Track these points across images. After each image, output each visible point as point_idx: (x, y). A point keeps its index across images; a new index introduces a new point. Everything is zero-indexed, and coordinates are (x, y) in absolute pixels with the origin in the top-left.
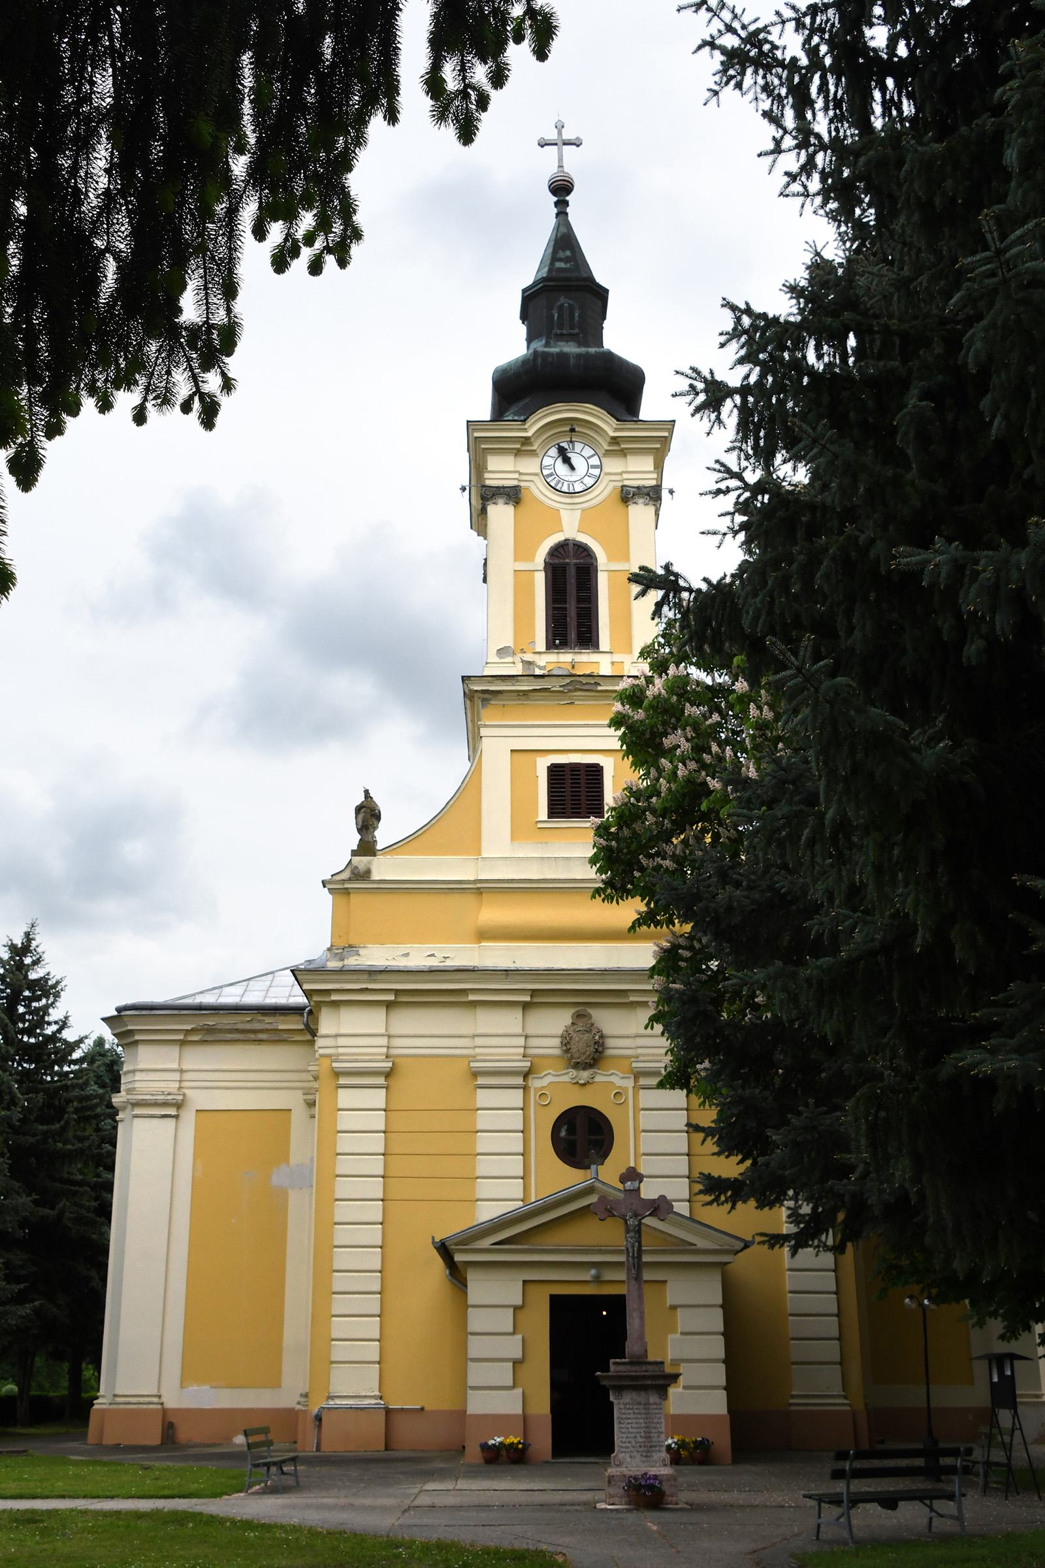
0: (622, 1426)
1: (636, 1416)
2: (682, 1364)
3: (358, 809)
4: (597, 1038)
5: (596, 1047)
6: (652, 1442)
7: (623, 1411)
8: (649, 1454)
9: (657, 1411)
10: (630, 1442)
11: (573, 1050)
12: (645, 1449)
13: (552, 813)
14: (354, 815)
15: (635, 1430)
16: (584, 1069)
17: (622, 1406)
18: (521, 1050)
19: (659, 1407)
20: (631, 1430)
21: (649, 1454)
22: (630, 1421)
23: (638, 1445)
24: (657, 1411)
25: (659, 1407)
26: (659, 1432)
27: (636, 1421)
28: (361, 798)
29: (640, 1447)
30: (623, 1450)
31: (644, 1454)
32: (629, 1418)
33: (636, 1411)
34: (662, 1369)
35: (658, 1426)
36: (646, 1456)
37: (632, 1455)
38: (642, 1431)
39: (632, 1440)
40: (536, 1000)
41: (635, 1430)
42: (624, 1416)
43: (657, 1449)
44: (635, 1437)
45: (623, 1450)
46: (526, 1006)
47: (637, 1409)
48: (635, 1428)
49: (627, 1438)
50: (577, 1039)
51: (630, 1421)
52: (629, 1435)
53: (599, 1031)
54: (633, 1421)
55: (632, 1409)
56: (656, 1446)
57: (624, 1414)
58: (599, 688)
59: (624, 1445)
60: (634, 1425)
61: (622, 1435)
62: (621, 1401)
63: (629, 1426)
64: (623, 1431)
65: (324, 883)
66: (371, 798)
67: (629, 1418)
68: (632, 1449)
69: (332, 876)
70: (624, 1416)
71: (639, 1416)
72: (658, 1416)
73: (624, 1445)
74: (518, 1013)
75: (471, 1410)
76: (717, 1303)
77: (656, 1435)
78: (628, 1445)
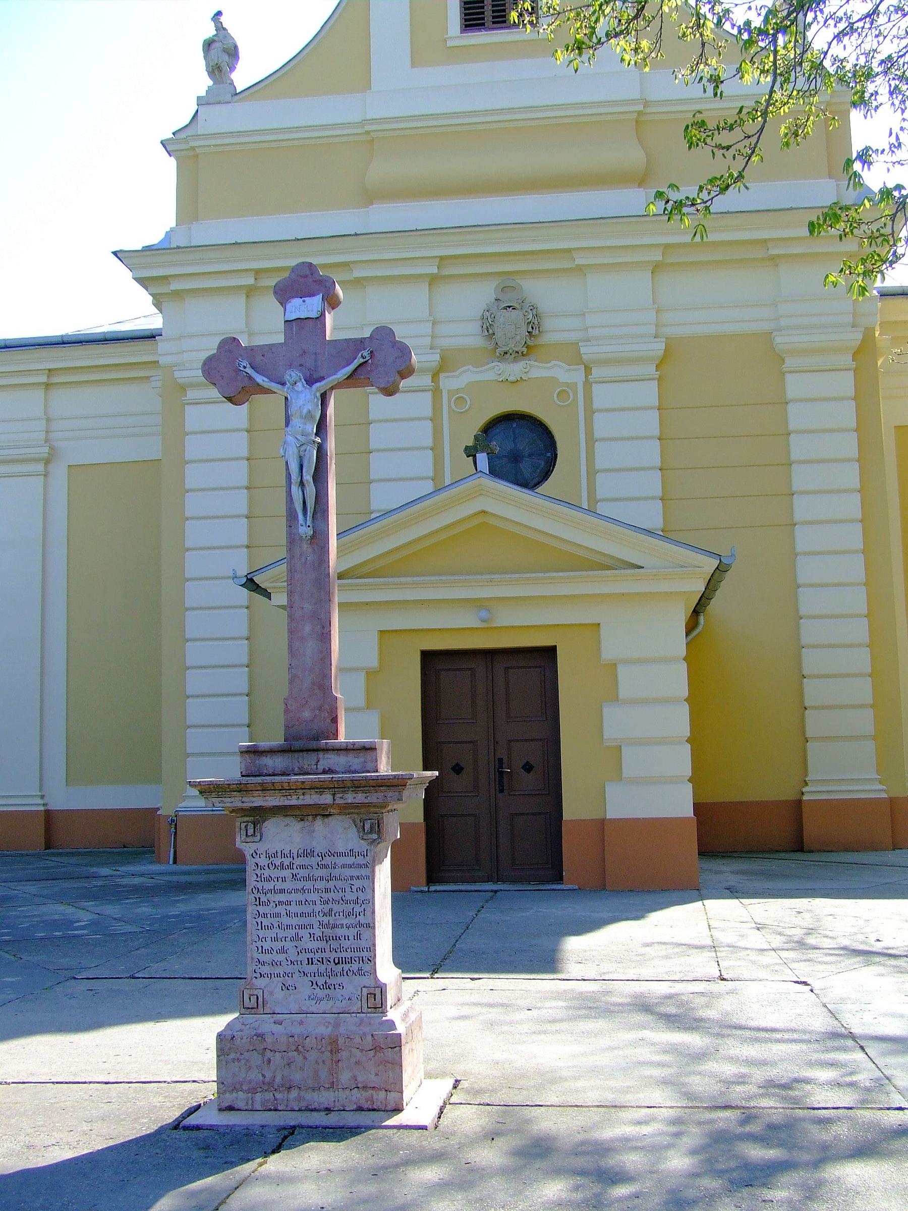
0: (262, 909)
1: (299, 885)
2: (282, 742)
3: (208, 45)
4: (530, 316)
5: (530, 329)
6: (341, 949)
7: (267, 873)
8: (332, 981)
9: (355, 872)
10: (283, 951)
11: (499, 334)
12: (322, 968)
13: (466, 26)
14: (202, 54)
15: (295, 921)
16: (515, 360)
17: (263, 861)
18: (428, 341)
19: (360, 860)
20: (286, 920)
21: (332, 981)
22: (282, 897)
23: (304, 957)
24: (355, 872)
25: (360, 860)
26: (360, 925)
27: (299, 897)
28: (210, 31)
29: (310, 961)
30: (265, 969)
31: (321, 981)
32: (282, 891)
33: (302, 873)
34: (369, 766)
35: (358, 909)
36: (326, 986)
37: (289, 981)
38: (314, 921)
39: (288, 945)
40: (446, 272)
41: (295, 921)
42: (269, 886)
43: (355, 967)
44: (297, 938)
45: (265, 969)
46: (433, 280)
47: (302, 867)
48: (296, 915)
49: (276, 939)
50: (502, 319)
51: (282, 897)
52: (282, 934)
53: (533, 308)
54: (294, 897)
55: (290, 867)
56: (351, 961)
57: (269, 879)
58: (712, 237)
59: (266, 958)
60: (293, 908)
61: (261, 933)
62: (262, 847)
63: (281, 909)
64: (266, 922)
65: (163, 143)
66: (225, 29)
67: (282, 891)
68: (289, 969)
69: (174, 134)
70: (269, 886)
71: (309, 885)
72: (357, 884)
73: (266, 958)
74: (422, 291)
75: (612, 813)
76: (43, 396)
77: (352, 932)
78: (281, 957)
